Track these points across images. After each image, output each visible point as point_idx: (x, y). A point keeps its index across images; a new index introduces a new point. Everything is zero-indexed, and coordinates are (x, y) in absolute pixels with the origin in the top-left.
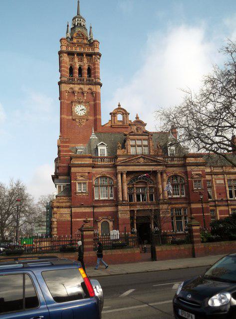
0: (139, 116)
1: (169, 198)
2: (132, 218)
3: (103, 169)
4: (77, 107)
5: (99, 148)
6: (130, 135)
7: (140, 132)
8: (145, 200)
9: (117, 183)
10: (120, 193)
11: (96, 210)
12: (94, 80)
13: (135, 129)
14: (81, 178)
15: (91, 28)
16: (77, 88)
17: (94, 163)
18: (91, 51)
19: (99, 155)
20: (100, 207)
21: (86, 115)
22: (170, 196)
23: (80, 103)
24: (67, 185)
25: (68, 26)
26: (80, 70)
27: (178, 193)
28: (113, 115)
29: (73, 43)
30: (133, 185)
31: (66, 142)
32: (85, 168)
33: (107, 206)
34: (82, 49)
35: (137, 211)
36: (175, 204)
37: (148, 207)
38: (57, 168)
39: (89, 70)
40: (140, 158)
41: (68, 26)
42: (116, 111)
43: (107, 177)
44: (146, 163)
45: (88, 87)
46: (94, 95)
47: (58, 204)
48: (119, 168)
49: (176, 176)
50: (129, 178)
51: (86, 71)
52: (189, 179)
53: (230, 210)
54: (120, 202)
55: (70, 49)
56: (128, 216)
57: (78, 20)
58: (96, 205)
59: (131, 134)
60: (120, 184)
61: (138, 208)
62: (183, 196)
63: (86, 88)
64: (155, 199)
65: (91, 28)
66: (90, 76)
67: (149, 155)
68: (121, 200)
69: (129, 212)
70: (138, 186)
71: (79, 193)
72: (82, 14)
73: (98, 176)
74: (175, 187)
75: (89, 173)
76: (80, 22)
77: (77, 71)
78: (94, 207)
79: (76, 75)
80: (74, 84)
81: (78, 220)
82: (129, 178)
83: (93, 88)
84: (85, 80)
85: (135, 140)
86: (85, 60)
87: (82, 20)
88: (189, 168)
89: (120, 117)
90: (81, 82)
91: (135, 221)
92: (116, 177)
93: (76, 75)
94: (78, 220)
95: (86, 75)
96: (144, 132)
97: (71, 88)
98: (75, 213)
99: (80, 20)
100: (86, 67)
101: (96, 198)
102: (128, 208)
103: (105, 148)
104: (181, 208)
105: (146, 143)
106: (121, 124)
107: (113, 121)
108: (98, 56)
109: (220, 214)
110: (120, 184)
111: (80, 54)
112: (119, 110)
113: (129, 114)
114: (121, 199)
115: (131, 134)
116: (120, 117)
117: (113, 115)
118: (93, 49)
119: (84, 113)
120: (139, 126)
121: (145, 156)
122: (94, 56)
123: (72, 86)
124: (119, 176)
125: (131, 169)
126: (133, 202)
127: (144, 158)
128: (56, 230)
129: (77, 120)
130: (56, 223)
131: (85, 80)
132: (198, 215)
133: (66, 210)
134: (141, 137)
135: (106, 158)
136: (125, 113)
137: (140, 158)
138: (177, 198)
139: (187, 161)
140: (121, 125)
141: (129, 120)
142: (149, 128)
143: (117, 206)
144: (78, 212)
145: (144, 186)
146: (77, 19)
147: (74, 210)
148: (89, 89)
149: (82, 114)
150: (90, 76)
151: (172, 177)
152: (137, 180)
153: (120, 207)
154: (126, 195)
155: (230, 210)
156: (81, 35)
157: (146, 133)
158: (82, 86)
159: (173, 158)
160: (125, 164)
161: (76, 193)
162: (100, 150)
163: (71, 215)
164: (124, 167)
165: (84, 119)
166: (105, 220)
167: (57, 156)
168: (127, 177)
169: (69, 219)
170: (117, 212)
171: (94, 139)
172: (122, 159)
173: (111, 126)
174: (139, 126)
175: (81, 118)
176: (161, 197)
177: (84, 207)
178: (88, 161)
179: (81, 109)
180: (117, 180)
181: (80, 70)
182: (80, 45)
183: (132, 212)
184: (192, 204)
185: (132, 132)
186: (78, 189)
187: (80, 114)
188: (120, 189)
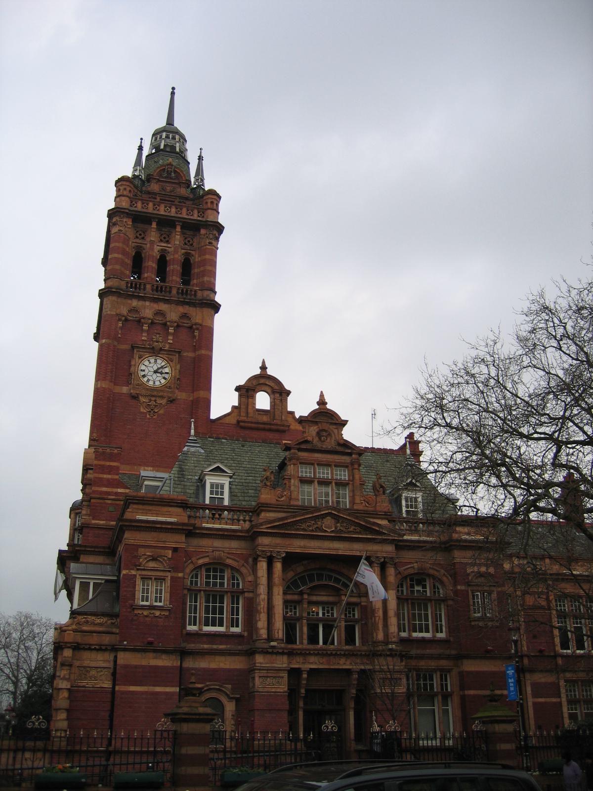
0: (327, 399)
1: (403, 641)
2: (292, 692)
3: (218, 543)
4: (147, 363)
5: (209, 480)
6: (300, 450)
7: (330, 444)
8: (333, 643)
9: (255, 584)
10: (263, 617)
11: (189, 663)
12: (199, 294)
13: (314, 433)
14: (152, 564)
15: (200, 158)
16: (148, 310)
17: (192, 521)
18: (195, 217)
19: (207, 502)
20: (203, 653)
21: (170, 388)
22: (404, 635)
23: (155, 352)
24: (107, 581)
25: (140, 148)
26: (162, 262)
27: (221, 620)
28: (246, 391)
29: (149, 193)
30: (301, 593)
31: (112, 457)
32: (163, 536)
33: (222, 653)
34: (173, 210)
35: (311, 672)
36: (421, 657)
37: (344, 664)
38: (76, 530)
39: (187, 266)
40: (324, 516)
41: (140, 148)
42: (255, 383)
43: (228, 566)
44: (341, 531)
45: (182, 309)
46: (196, 333)
47: (79, 638)
48: (264, 541)
49: (419, 578)
50: (290, 574)
51: (178, 268)
52: (459, 587)
53: (562, 683)
54: (260, 645)
55: (139, 206)
56: (282, 687)
57: (167, 137)
58: (191, 646)
59: (303, 446)
60: (262, 590)
61: (314, 663)
62: (441, 635)
63: (173, 313)
64: (362, 638)
65: (200, 158)
66: (186, 282)
67: (352, 512)
68: (265, 636)
69: (285, 675)
70: (314, 598)
71: (143, 608)
72: (178, 124)
73: (201, 562)
74: (214, 602)
75: (175, 550)
76: (173, 142)
77: (151, 264)
78: (184, 654)
79: (150, 274)
80: (143, 298)
81: (133, 688)
82: (290, 574)
83: (197, 316)
84: (174, 291)
85: (313, 464)
86: (177, 238)
87: (177, 137)
88: (459, 556)
89: (263, 401)
90: (161, 294)
91: (301, 704)
92: (254, 571)
93: (150, 274)
94: (133, 688)
95: (175, 278)
96: (339, 444)
97: (134, 310)
98: (126, 667)
99: (174, 138)
100: (179, 256)
101: (390, 640)
102: (282, 662)
103: (226, 481)
104: (435, 671)
105: (343, 475)
106: (265, 419)
107: (243, 410)
108: (215, 232)
109: (535, 695)
110: (262, 590)
111: (166, 224)
112: (262, 381)
113: (288, 393)
114: (263, 633)
115: (303, 446)
116: (263, 401)
117: (244, 391)
118: (202, 212)
119: (163, 381)
120: (325, 426)
121: (339, 511)
122: (203, 231)
123: (135, 303)
124: (263, 566)
125: (298, 546)
126: (298, 646)
127: (336, 518)
128: (63, 715)
129: (142, 399)
130: (66, 694)
131: (174, 291)
132: (548, 700)
133: (100, 656)
134: (329, 457)
135: (229, 509)
136: (279, 393)
137: (324, 516)
138: (423, 640)
139: (455, 536)
140: (264, 424)
141: (289, 409)
142: (353, 435)
143: (251, 653)
144: (136, 667)
145: (331, 599)
146: (164, 135)
147: (124, 658)
148: (184, 316)
149: (157, 383)
150: (186, 282)
151: (411, 577)
152: (311, 580)
153: (259, 659)
154: (279, 624)
155: (562, 683)
156: (173, 175)
157: (347, 448)
158: (163, 307)
159: (413, 522)
160: (283, 531)
161: (133, 607)
162: (212, 485)
163: (114, 674)
164: (278, 540)
165: (162, 397)
166: (214, 695)
167: (79, 496)
168: (285, 569)
169: (107, 684)
170: (251, 671)
171: (193, 454)
172: (272, 515)
173: (238, 422)
174: (325, 426)
175: (154, 393)
176: (380, 636)
177: (155, 651)
178: (171, 517)
179: (155, 368)
180: (256, 577)
181: (162, 262)
182: (168, 199)
183: (294, 673)
184: (465, 662)
185: (306, 442)
186: (139, 595)
187: (151, 383)
188: (263, 605)
